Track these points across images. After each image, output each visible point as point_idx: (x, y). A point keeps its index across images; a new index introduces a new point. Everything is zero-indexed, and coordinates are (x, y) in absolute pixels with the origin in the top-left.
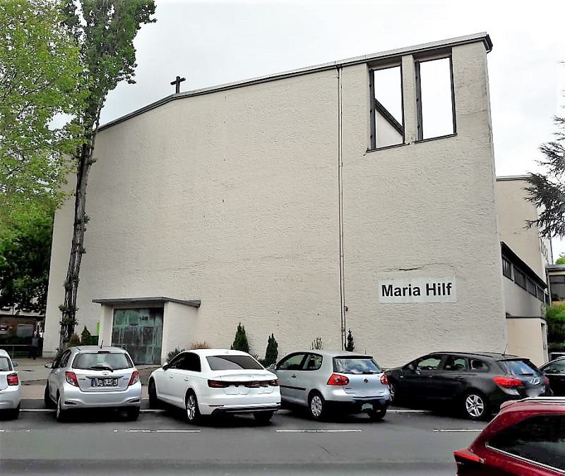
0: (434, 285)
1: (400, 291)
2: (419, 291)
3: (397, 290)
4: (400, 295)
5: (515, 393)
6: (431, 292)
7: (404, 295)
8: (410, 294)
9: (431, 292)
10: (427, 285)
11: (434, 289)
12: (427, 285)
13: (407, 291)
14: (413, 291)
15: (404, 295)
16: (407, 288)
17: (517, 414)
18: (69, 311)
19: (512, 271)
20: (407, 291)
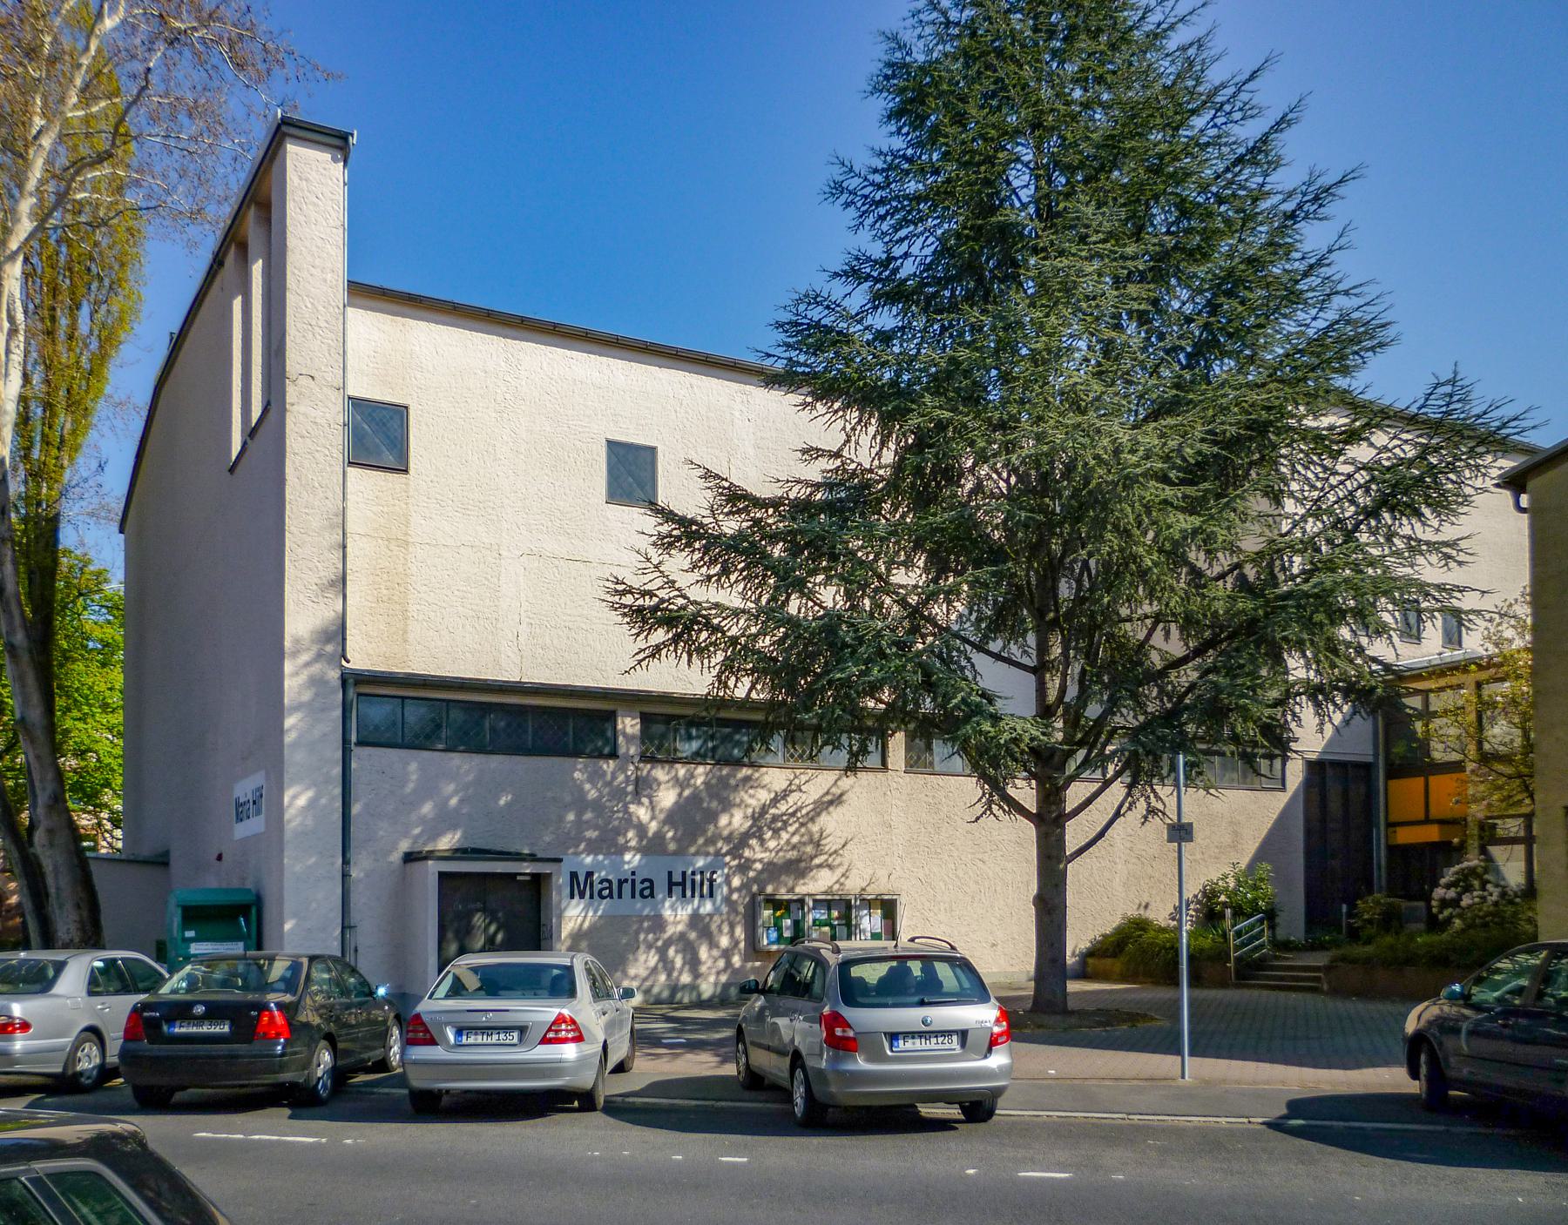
0: (684, 873)
1: (610, 888)
2: (652, 888)
3: (606, 884)
4: (611, 895)
5: (954, 1112)
6: (677, 878)
7: (620, 896)
8: (633, 896)
9: (677, 878)
10: (670, 874)
11: (683, 884)
12: (670, 874)
13: (627, 888)
14: (639, 887)
15: (620, 896)
16: (626, 881)
17: (556, 972)
18: (1442, 689)
19: (694, 1103)
20: (627, 888)
